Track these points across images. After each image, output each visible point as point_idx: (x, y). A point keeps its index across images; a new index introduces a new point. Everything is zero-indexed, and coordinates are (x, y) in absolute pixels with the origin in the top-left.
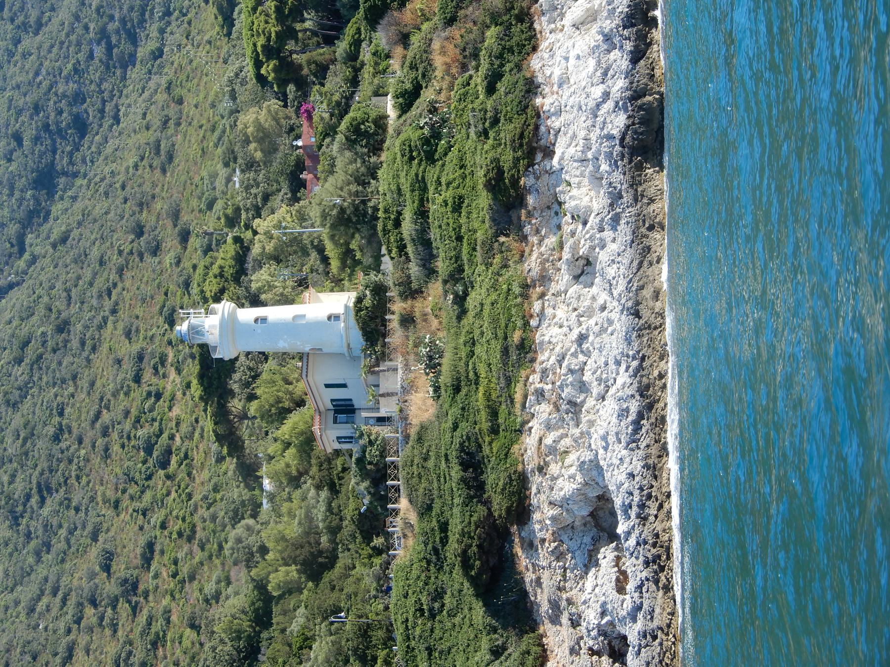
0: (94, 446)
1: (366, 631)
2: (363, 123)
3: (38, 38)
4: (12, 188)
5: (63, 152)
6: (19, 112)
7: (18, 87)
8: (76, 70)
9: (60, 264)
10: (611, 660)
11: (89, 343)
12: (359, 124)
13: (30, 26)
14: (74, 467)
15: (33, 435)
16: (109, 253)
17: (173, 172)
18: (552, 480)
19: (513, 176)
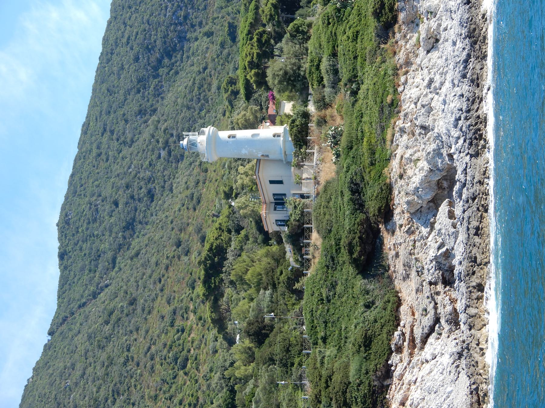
0: (145, 367)
1: (288, 348)
2: (301, 26)
3: (131, 149)
4: (111, 231)
5: (140, 211)
6: (118, 190)
7: (118, 175)
8: (150, 165)
9: (134, 268)
10: (443, 286)
11: (147, 310)
12: (299, 27)
13: (127, 143)
14: (133, 380)
15: (112, 364)
16: (161, 259)
17: (200, 210)
18: (408, 179)
19: (391, 4)
